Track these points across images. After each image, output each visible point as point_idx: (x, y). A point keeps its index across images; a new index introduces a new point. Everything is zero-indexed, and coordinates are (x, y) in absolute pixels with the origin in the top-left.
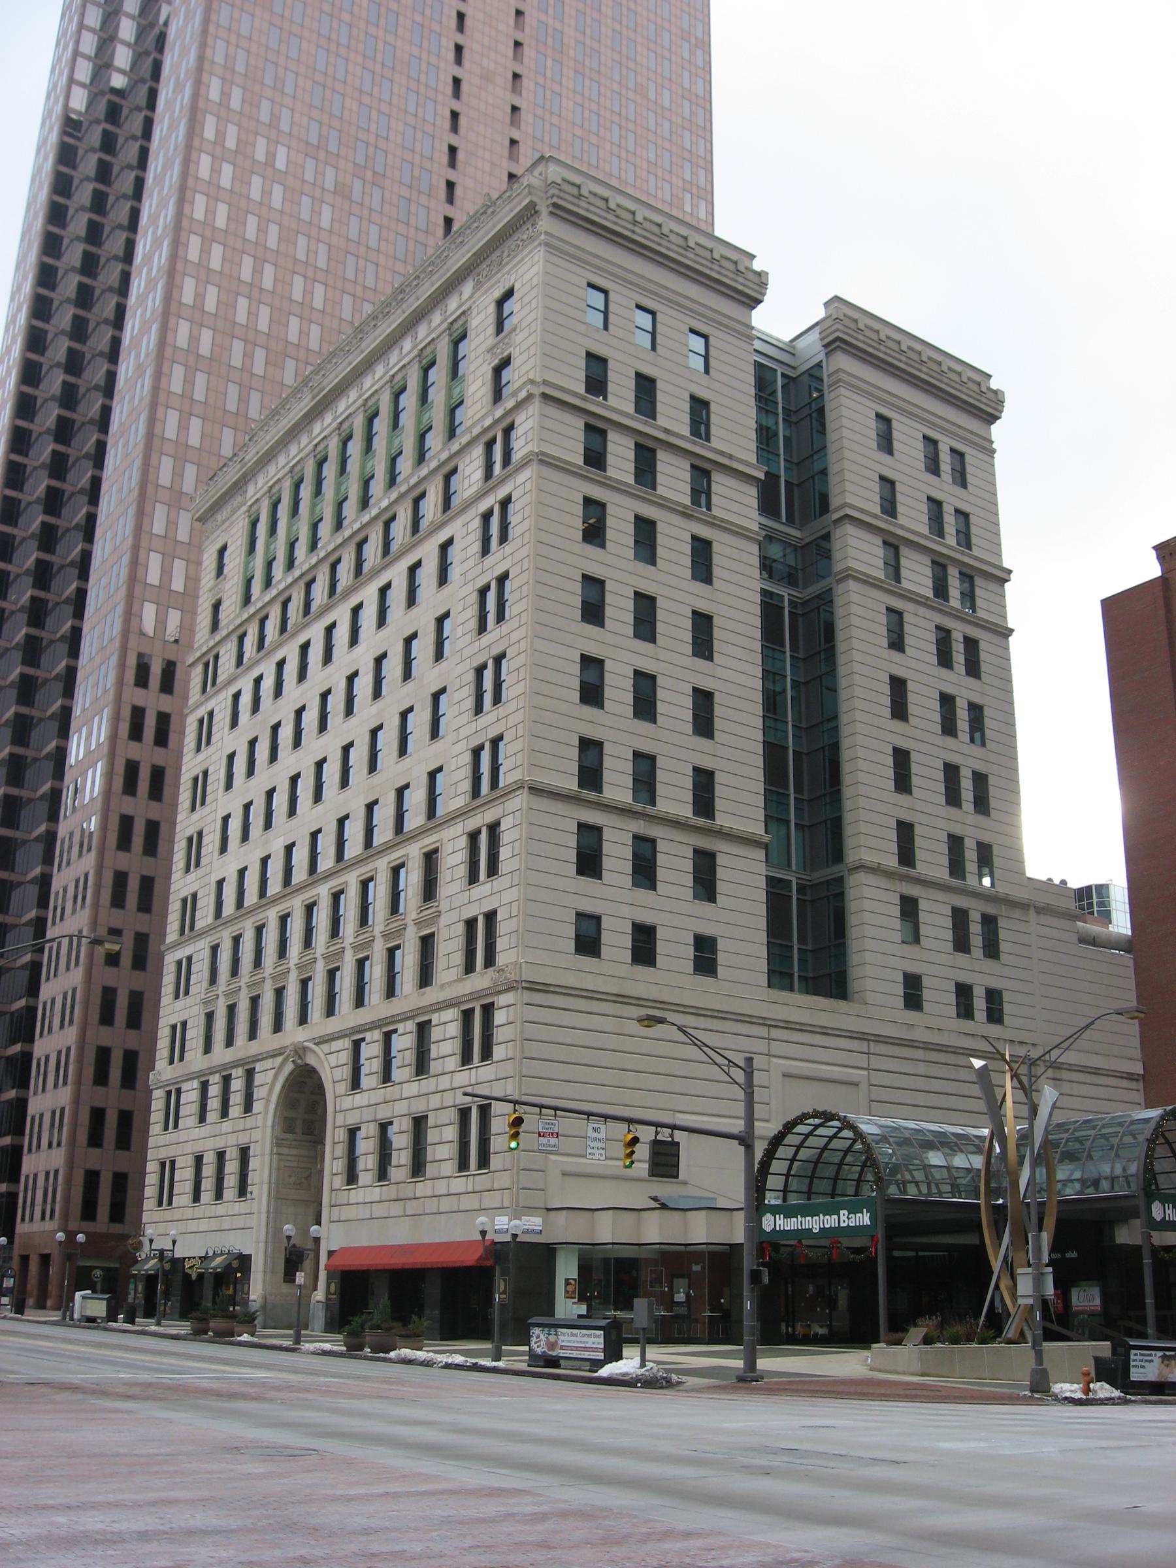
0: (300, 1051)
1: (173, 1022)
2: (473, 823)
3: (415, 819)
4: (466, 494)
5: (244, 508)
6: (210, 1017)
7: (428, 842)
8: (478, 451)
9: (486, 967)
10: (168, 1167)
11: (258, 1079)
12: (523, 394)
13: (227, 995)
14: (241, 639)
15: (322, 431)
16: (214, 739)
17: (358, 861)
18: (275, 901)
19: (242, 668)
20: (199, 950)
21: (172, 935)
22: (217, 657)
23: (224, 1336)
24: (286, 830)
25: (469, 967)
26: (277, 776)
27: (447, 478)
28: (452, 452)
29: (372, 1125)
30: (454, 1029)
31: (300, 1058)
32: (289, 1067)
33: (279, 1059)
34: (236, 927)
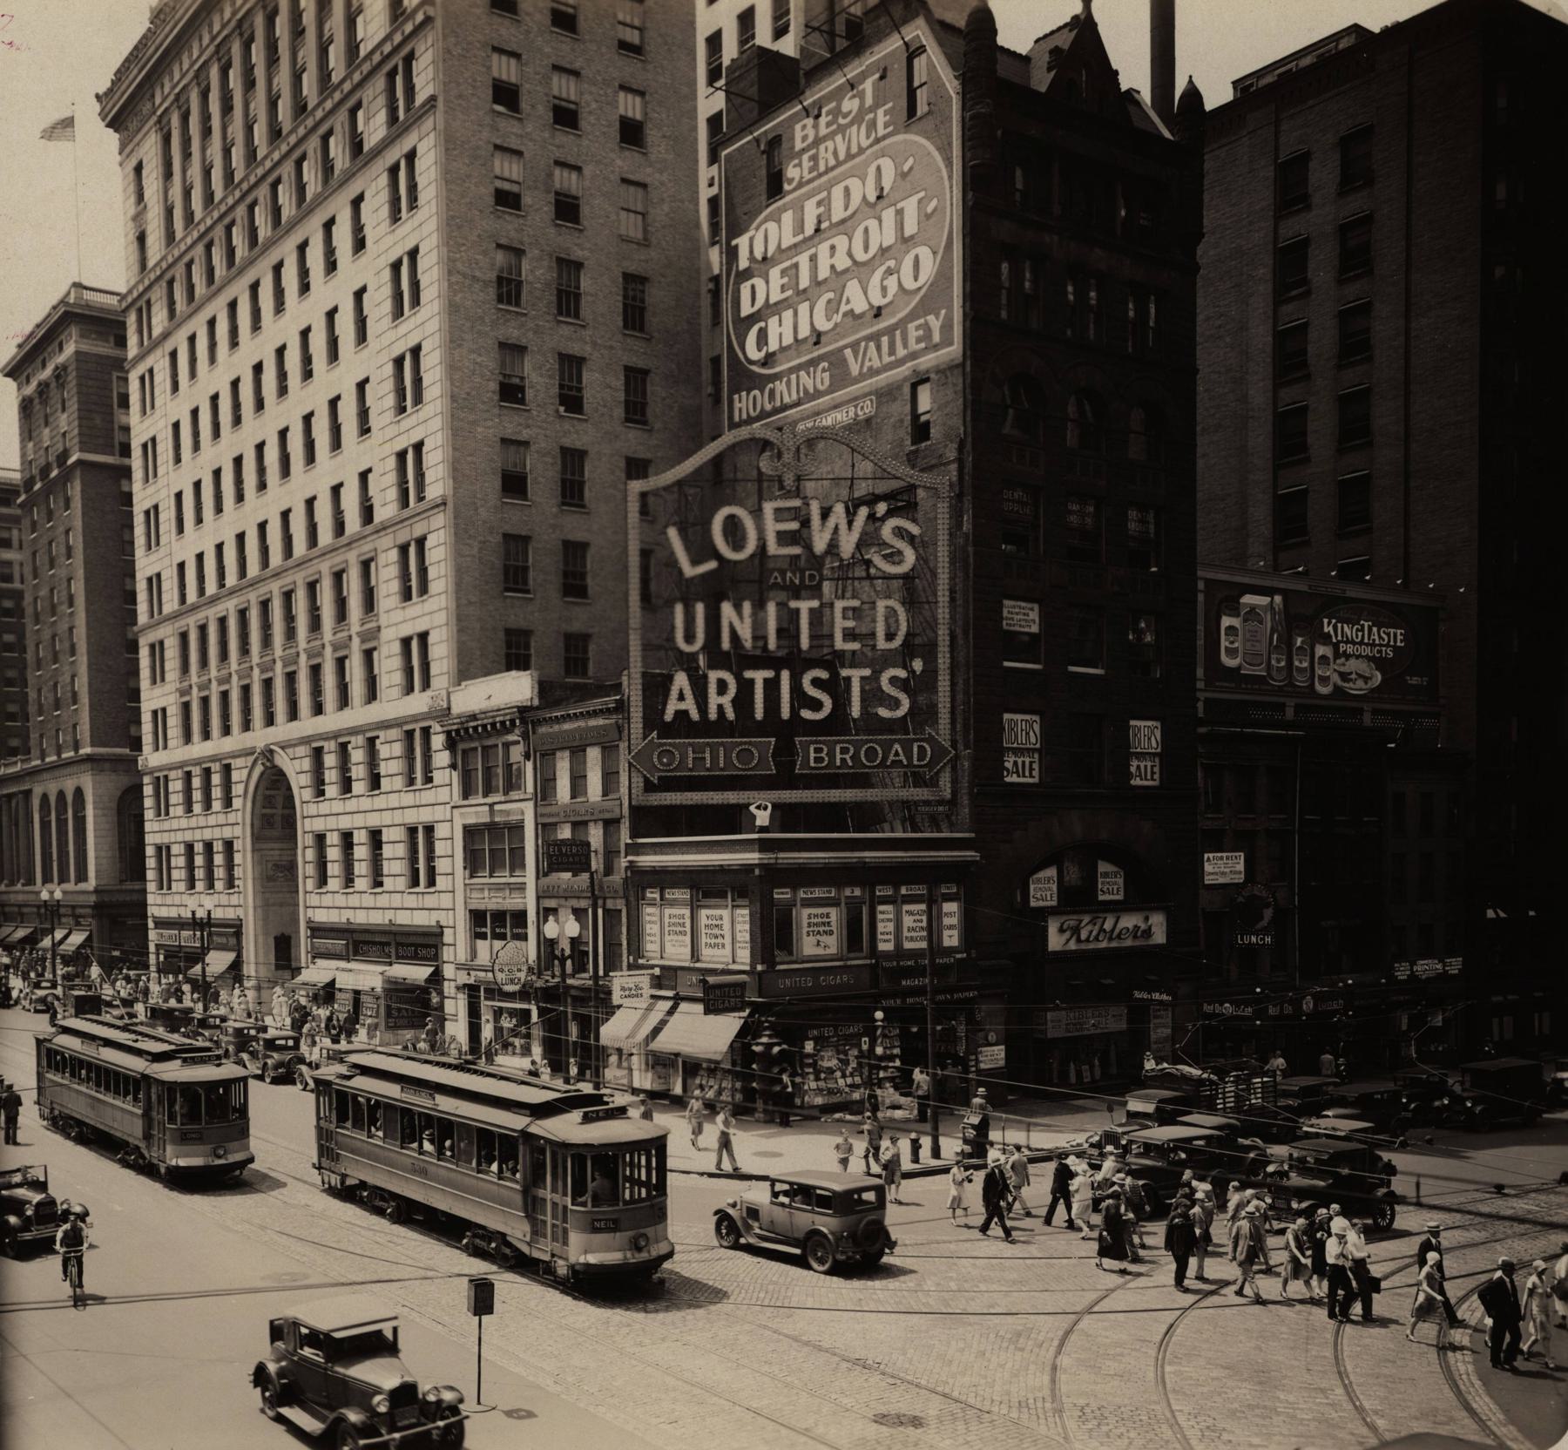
0: (268, 754)
1: (154, 708)
2: (403, 536)
3: (386, 508)
4: (373, 143)
5: (155, 118)
6: (186, 707)
7: (366, 548)
8: (380, 83)
9: (424, 690)
10: (163, 851)
11: (235, 776)
12: (420, 17)
13: (221, 682)
14: (171, 283)
15: (223, 26)
16: (157, 403)
17: (175, 616)
18: (253, 584)
19: (257, 249)
20: (168, 634)
21: (143, 617)
22: (149, 303)
23: (785, 1123)
24: (330, 467)
25: (409, 689)
26: (236, 442)
27: (353, 112)
28: (417, 22)
29: (336, 833)
30: (398, 749)
31: (268, 760)
32: (259, 769)
33: (251, 759)
34: (243, 599)
